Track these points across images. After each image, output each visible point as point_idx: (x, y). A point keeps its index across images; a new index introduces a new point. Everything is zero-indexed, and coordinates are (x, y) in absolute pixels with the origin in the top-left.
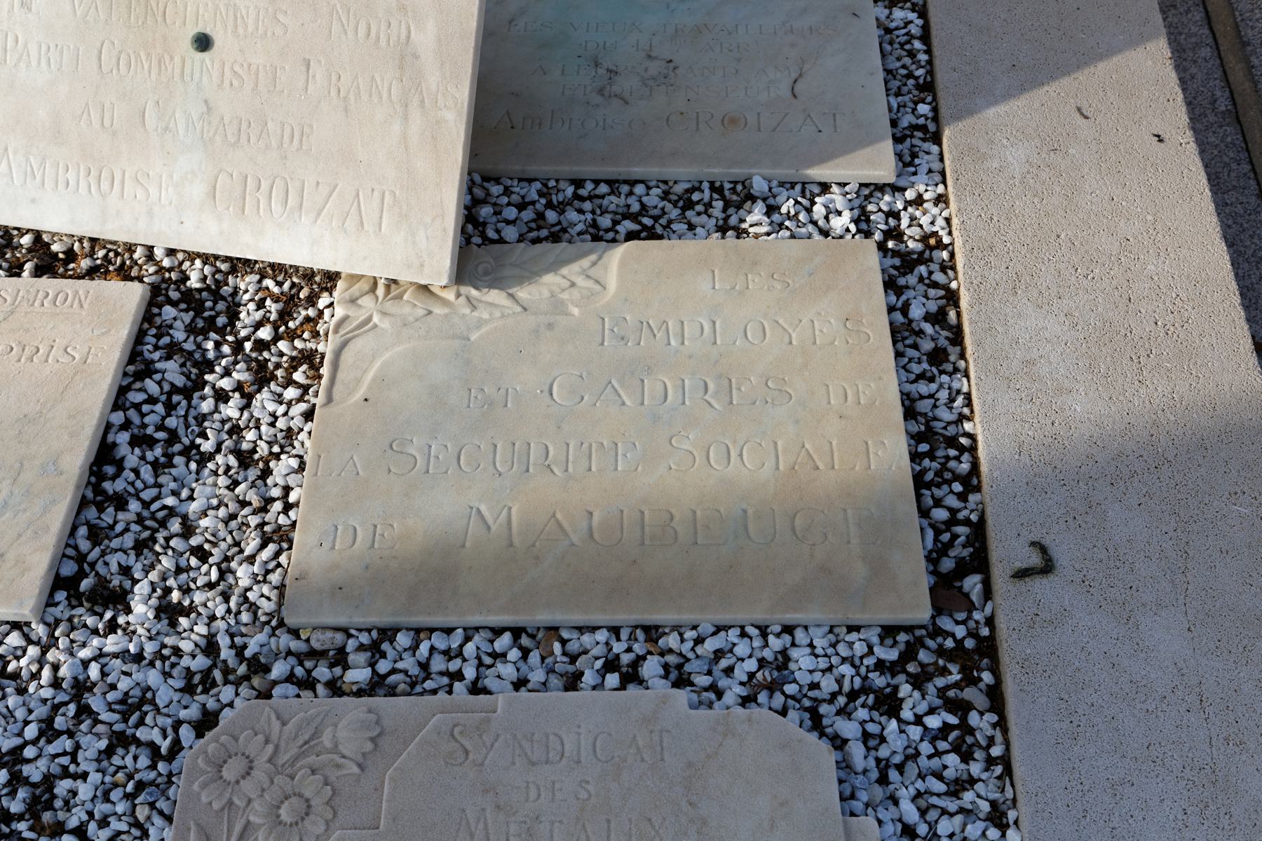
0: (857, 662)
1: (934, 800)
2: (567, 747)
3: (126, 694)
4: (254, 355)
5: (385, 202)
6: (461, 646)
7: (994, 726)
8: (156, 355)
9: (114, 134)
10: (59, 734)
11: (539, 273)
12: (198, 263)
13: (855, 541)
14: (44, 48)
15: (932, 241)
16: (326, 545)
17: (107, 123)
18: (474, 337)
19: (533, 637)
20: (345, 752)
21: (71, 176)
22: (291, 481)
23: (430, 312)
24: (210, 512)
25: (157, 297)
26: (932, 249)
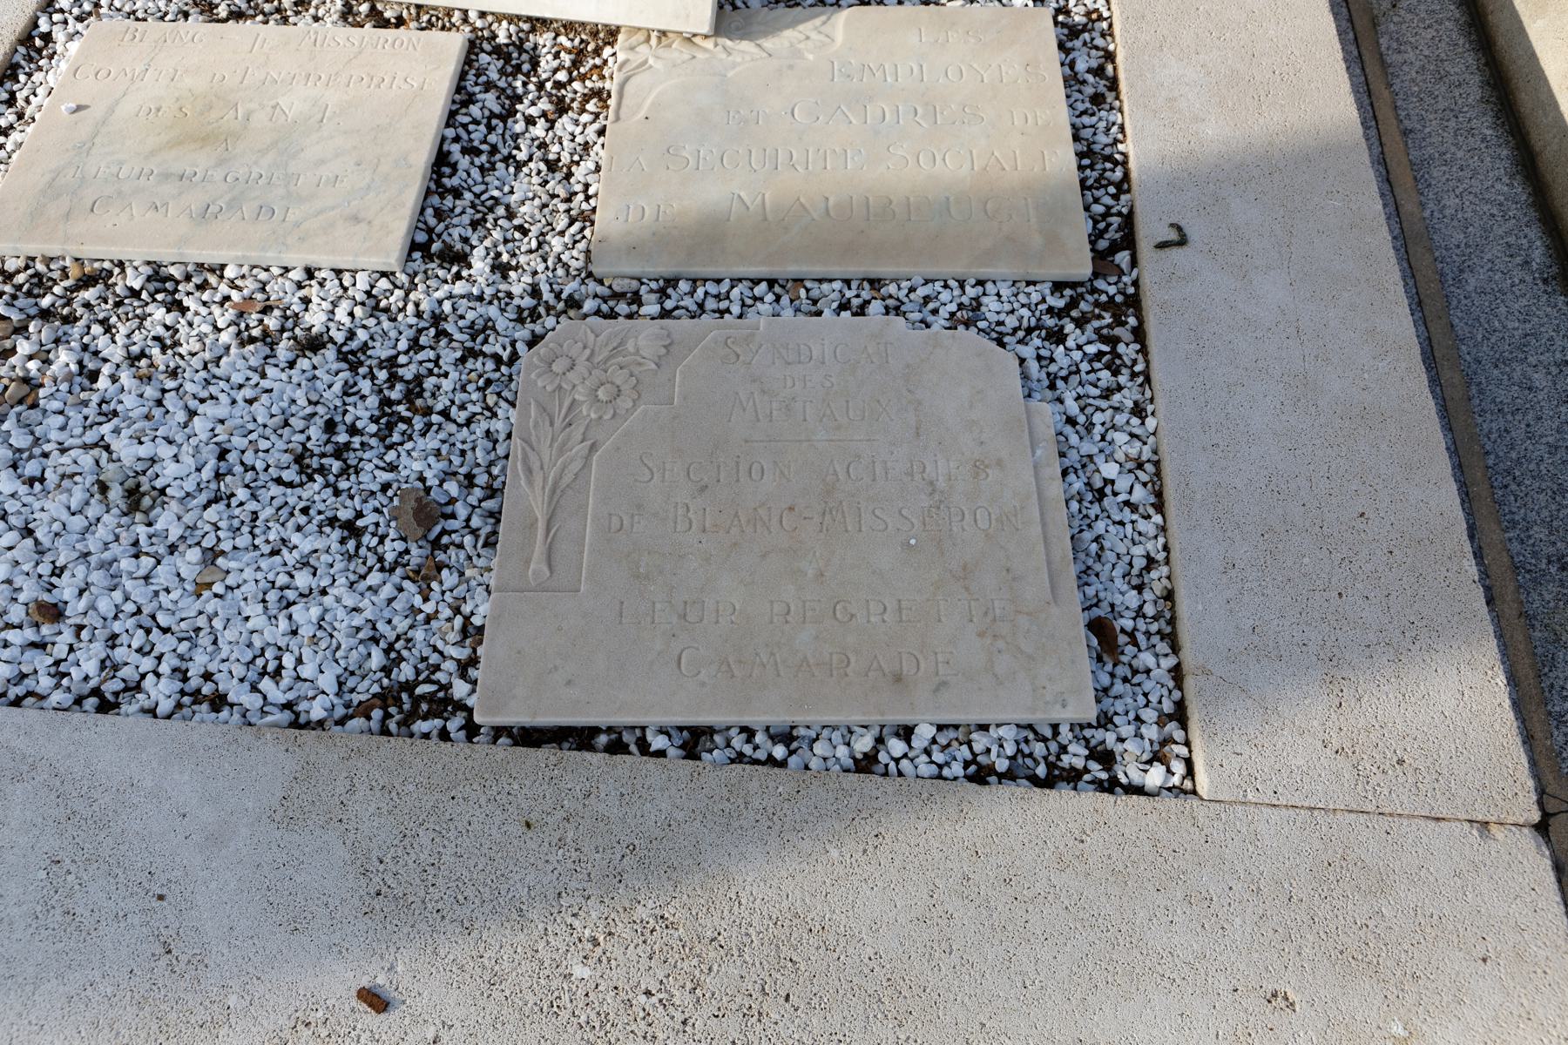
0: (1033, 308)
1: (1091, 401)
2: (814, 353)
3: (473, 322)
4: (554, 92)
6: (728, 292)
7: (1137, 352)
8: (477, 89)
10: (423, 348)
11: (780, 29)
12: (505, 23)
13: (1033, 220)
15: (1094, 16)
16: (622, 219)
18: (730, 74)
19: (783, 287)
20: (644, 354)
22: (590, 179)
23: (694, 57)
25: (473, 47)
26: (1094, 21)
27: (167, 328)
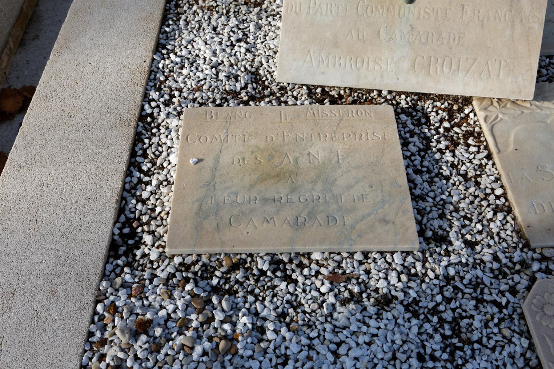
3: (470, 280)
5: (502, 65)
9: (364, 42)
14: (329, 6)
17: (361, 37)
18: (549, 121)
21: (342, 61)
23: (523, 112)
24: (462, 201)
27: (292, 294)
